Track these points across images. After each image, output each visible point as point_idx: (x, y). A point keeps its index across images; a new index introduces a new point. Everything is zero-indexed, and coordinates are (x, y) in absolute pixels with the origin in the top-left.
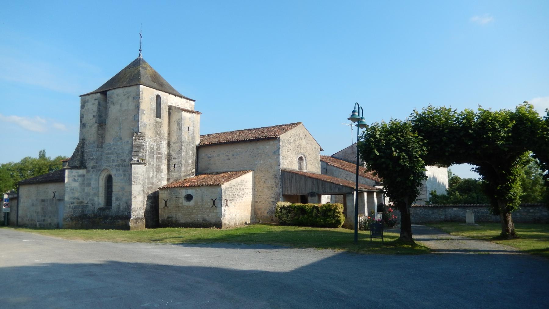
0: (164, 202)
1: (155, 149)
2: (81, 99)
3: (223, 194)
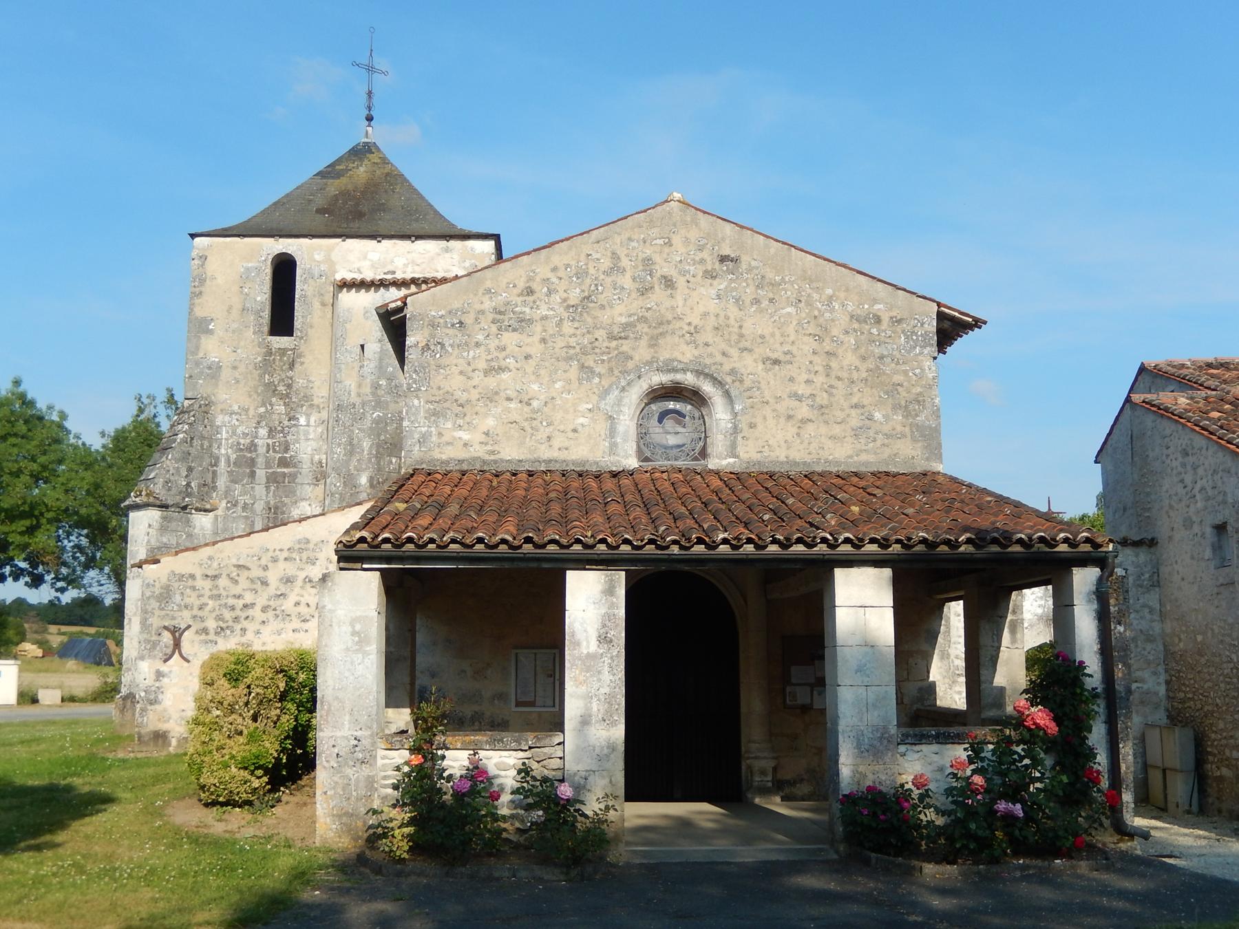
1: (262, 450)
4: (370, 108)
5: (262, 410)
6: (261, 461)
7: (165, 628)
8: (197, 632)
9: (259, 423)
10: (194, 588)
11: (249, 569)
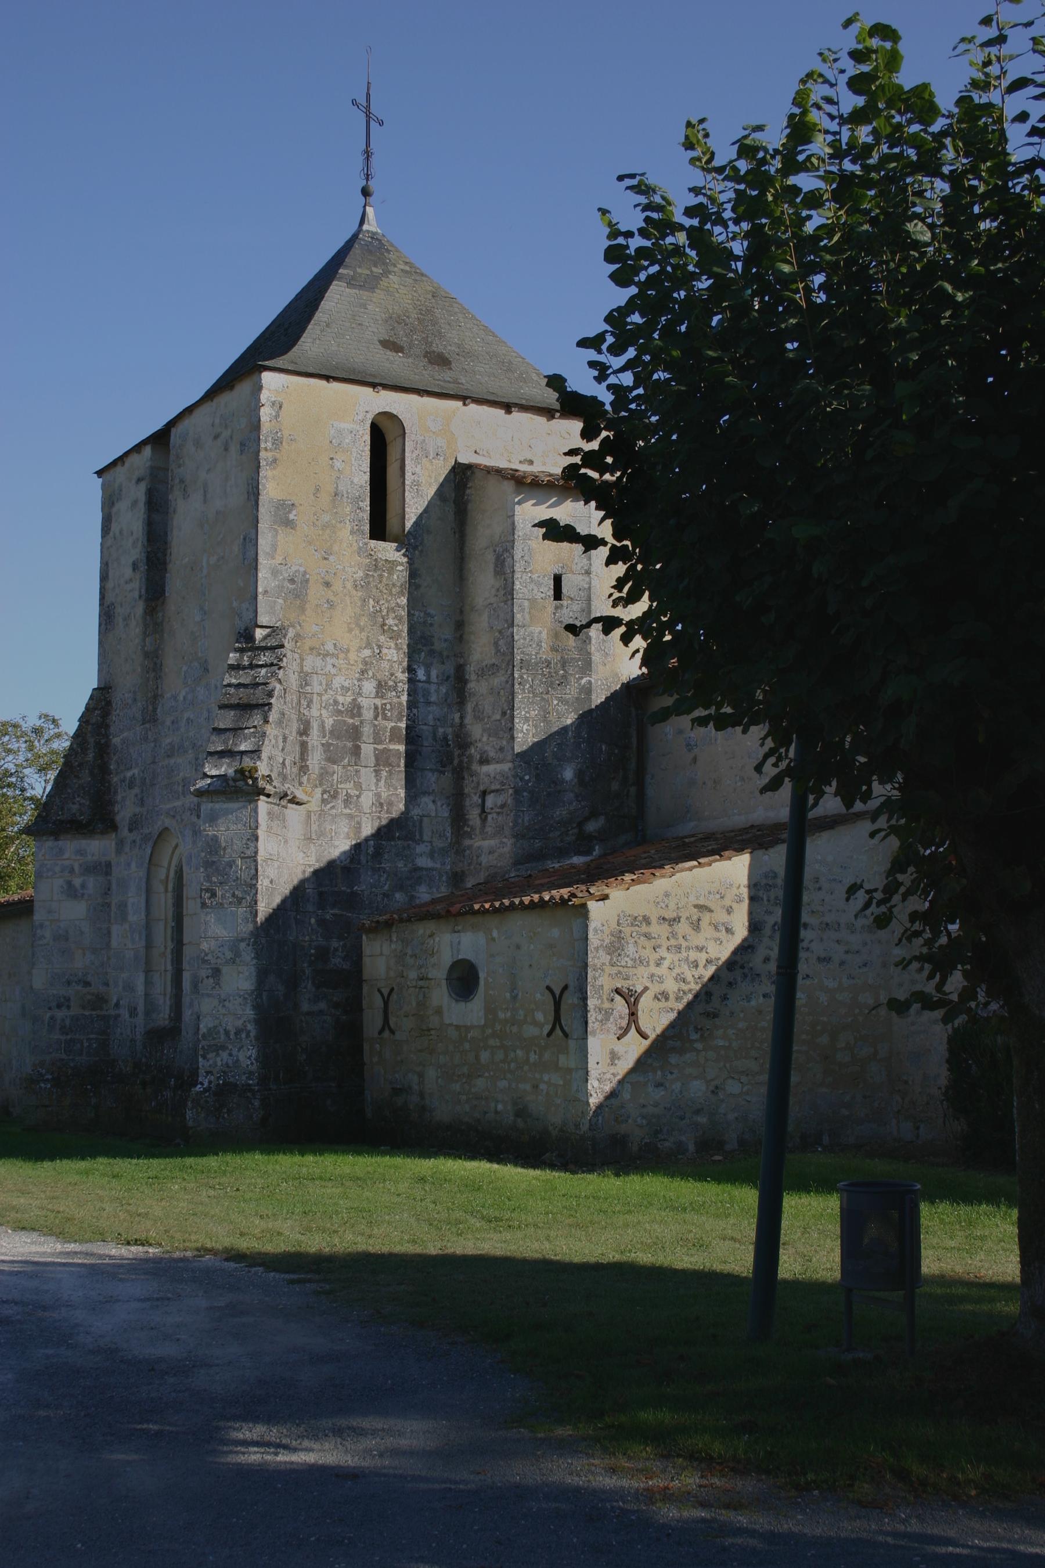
0: (379, 1002)
1: (368, 714)
2: (104, 487)
3: (597, 958)
4: (368, 177)
5: (367, 652)
6: (367, 730)
7: (618, 991)
8: (656, 997)
9: (363, 672)
10: (648, 936)
11: (711, 911)
